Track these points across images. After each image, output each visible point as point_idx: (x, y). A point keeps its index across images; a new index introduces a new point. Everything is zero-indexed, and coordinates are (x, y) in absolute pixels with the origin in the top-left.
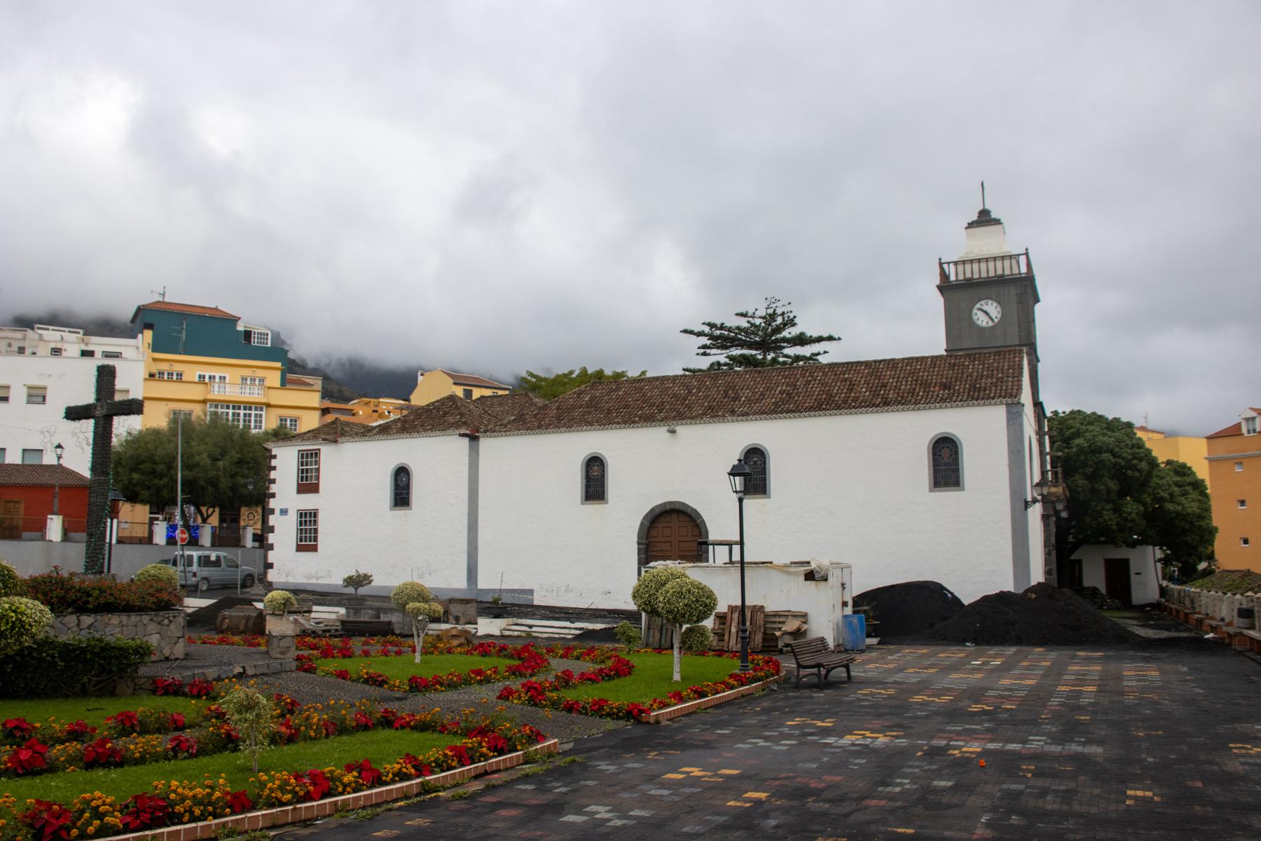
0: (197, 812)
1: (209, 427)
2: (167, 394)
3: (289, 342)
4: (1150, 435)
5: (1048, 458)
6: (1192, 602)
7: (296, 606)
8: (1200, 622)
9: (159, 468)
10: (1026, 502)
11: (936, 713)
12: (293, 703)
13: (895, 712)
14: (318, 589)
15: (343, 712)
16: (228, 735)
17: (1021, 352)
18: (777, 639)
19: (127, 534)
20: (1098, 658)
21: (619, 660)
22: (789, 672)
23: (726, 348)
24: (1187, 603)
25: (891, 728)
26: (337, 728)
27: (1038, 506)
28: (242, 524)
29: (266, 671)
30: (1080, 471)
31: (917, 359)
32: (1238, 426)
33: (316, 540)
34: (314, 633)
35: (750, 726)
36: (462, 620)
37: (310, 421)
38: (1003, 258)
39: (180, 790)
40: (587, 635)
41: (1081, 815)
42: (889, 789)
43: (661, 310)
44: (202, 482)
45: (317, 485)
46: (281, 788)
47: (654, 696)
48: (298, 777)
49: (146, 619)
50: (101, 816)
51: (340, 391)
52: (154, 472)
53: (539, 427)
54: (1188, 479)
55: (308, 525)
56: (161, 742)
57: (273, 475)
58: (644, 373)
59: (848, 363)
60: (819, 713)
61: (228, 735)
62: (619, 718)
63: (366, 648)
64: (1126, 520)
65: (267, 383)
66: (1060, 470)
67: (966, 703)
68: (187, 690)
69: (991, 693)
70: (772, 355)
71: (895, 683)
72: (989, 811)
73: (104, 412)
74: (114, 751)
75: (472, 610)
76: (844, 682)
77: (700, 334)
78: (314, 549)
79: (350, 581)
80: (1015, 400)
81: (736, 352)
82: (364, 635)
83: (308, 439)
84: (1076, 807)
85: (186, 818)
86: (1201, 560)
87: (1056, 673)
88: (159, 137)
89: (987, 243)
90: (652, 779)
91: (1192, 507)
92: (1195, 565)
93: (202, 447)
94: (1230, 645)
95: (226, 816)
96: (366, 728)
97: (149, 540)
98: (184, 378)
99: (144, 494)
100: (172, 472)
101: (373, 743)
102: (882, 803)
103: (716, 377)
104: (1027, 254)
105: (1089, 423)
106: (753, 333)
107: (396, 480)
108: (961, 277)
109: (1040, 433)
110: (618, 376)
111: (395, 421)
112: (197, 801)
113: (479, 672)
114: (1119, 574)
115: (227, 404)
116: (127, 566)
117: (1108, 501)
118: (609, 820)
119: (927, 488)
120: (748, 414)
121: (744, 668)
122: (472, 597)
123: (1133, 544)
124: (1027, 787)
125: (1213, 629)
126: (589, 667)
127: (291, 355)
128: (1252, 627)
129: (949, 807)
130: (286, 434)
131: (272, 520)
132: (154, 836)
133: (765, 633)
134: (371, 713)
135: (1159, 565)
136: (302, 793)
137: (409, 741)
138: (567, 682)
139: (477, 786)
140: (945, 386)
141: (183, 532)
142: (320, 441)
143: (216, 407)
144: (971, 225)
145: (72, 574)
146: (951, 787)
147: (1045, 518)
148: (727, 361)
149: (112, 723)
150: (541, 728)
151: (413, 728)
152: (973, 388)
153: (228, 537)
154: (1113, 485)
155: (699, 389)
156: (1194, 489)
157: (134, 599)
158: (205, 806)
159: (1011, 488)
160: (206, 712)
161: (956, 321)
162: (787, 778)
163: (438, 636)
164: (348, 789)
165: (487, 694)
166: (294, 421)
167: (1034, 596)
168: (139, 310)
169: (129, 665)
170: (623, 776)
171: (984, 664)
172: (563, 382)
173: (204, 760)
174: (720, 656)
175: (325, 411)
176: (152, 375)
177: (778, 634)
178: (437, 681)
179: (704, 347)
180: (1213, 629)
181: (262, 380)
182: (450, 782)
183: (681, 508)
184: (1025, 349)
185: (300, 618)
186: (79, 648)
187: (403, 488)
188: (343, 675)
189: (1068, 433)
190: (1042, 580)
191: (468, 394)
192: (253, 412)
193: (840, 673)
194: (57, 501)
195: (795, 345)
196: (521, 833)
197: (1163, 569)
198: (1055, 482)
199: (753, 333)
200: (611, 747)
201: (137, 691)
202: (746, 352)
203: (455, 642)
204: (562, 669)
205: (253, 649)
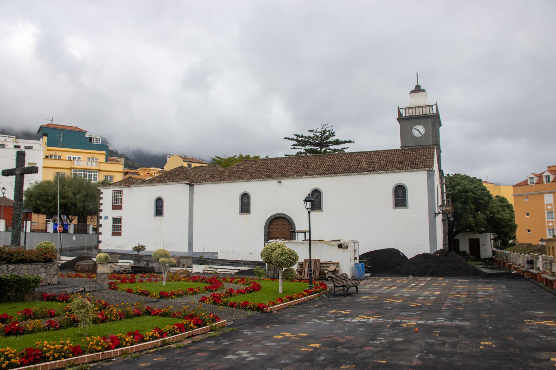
0: (56, 356)
1: (73, 180)
2: (47, 166)
3: (110, 142)
4: (489, 185)
5: (445, 194)
6: (507, 257)
7: (111, 260)
8: (510, 266)
9: (50, 198)
10: (435, 214)
11: (395, 307)
12: (106, 304)
13: (378, 307)
14: (122, 252)
15: (128, 308)
16: (74, 319)
17: (433, 148)
18: (325, 274)
19: (35, 228)
20: (467, 282)
21: (255, 284)
22: (331, 289)
23: (304, 145)
24: (505, 257)
25: (376, 314)
26: (124, 316)
27: (441, 216)
28: (88, 223)
29: (94, 289)
31: (388, 150)
32: (526, 181)
33: (120, 230)
34: (119, 272)
35: (313, 313)
36: (186, 266)
37: (119, 177)
38: (426, 106)
39: (48, 346)
40: (241, 272)
41: (460, 354)
42: (375, 342)
43: (275, 129)
44: (69, 205)
45: (121, 206)
46: (96, 344)
47: (270, 300)
48: (105, 339)
49: (39, 266)
50: (9, 359)
51: (133, 164)
52: (47, 200)
53: (220, 180)
54: (505, 204)
55: (117, 224)
56: (41, 323)
57: (101, 201)
58: (267, 156)
59: (357, 152)
60: (344, 308)
61: (74, 319)
62: (254, 310)
63: (141, 278)
64: (478, 222)
65: (99, 161)
66: (450, 200)
67: (409, 302)
68: (57, 298)
69: (420, 298)
70: (324, 149)
71: (378, 293)
72: (419, 352)
73: (20, 172)
74: (19, 328)
75: (190, 261)
76: (355, 293)
77: (292, 139)
78: (120, 234)
79: (136, 249)
80: (431, 169)
81: (308, 147)
82: (141, 273)
83: (117, 185)
84: (458, 350)
85: (51, 359)
86: (510, 239)
87: (448, 289)
88: (49, 49)
89: (419, 100)
90: (268, 338)
91: (506, 216)
92: (508, 241)
93: (69, 189)
94: (523, 276)
95: (70, 357)
96: (138, 315)
97: (45, 231)
98: (62, 158)
99: (43, 210)
100: (56, 200)
101: (141, 322)
102: (372, 349)
103: (299, 158)
104: (436, 105)
105: (463, 179)
106: (316, 139)
107: (156, 204)
108: (407, 115)
109: (441, 183)
110: (256, 158)
111: (156, 177)
112: (56, 351)
113: (191, 289)
114: (475, 245)
115: (81, 170)
116: (32, 242)
117: (471, 214)
118: (248, 357)
119: (161, 218)
120: (313, 175)
121: (311, 287)
122: (191, 256)
124: (436, 341)
125: (516, 269)
126: (241, 287)
127: (110, 148)
128: (533, 268)
129: (401, 350)
130: (107, 183)
131: (101, 222)
132: (35, 368)
133: (320, 272)
134: (141, 309)
135: (492, 241)
136: (106, 346)
137: (158, 321)
138: (231, 294)
139: (188, 342)
140: (400, 163)
141: (60, 227)
142: (123, 186)
143: (76, 171)
145: (5, 246)
146: (403, 341)
147: (443, 220)
148: (304, 151)
149: (20, 314)
150: (218, 315)
151: (160, 315)
152: (413, 163)
153: (81, 229)
154: (473, 207)
155: (292, 164)
157: (33, 257)
158: (60, 353)
159: (429, 208)
160: (65, 309)
161: (405, 134)
162: (329, 337)
163: (175, 273)
164: (128, 344)
165: (195, 299)
166: (112, 177)
167: (438, 255)
168: (41, 127)
169: (30, 287)
170: (255, 337)
171: (417, 285)
172: (231, 160)
173: (62, 331)
174: (300, 281)
175: (126, 173)
176: (47, 157)
177: (326, 272)
178: (172, 294)
179: (294, 145)
180: (516, 269)
181: (97, 159)
182: (176, 340)
183: (284, 216)
184: (435, 147)
185: (113, 265)
186: (6, 280)
187: (160, 207)
188: (130, 291)
189: (453, 184)
190: (442, 248)
191: (190, 166)
192: (93, 174)
193: (353, 289)
194: (2, 213)
195: (334, 144)
196: (207, 364)
197: (494, 243)
198: (448, 205)
199: (316, 139)
200: (250, 323)
201: (34, 299)
202: (313, 147)
203: (182, 276)
204: (229, 288)
205: (90, 280)
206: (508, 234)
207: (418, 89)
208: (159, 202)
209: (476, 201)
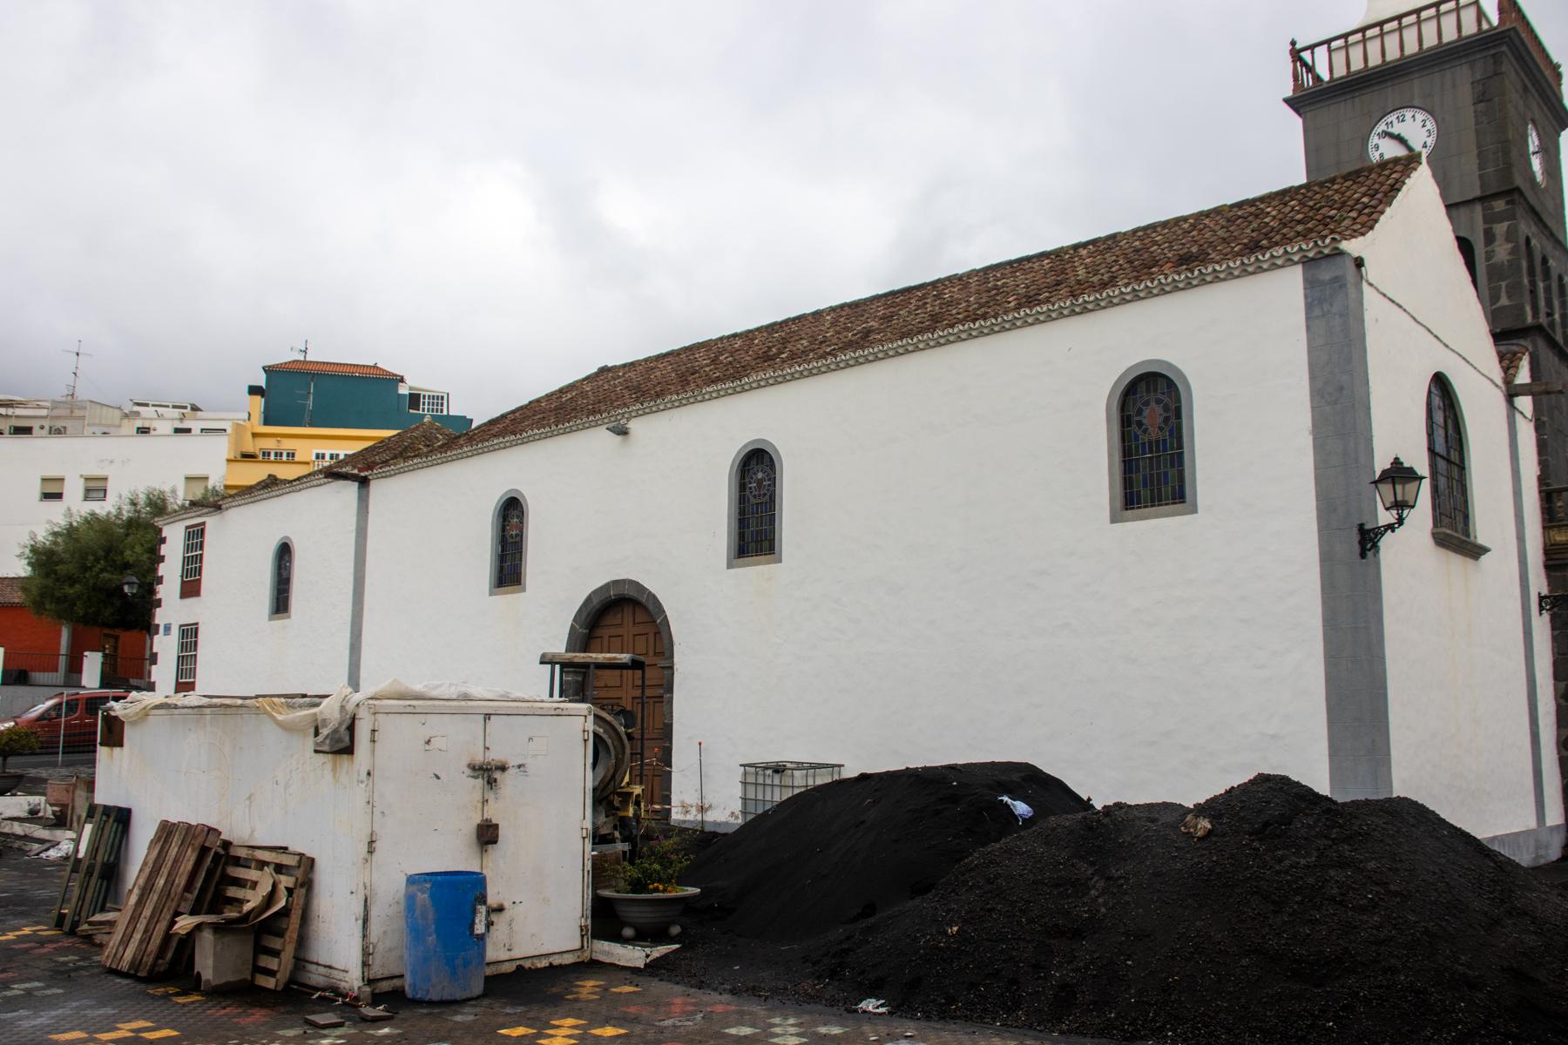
98: (297, 459)
108: (1340, 71)
119: (286, 621)
167: (1205, 824)
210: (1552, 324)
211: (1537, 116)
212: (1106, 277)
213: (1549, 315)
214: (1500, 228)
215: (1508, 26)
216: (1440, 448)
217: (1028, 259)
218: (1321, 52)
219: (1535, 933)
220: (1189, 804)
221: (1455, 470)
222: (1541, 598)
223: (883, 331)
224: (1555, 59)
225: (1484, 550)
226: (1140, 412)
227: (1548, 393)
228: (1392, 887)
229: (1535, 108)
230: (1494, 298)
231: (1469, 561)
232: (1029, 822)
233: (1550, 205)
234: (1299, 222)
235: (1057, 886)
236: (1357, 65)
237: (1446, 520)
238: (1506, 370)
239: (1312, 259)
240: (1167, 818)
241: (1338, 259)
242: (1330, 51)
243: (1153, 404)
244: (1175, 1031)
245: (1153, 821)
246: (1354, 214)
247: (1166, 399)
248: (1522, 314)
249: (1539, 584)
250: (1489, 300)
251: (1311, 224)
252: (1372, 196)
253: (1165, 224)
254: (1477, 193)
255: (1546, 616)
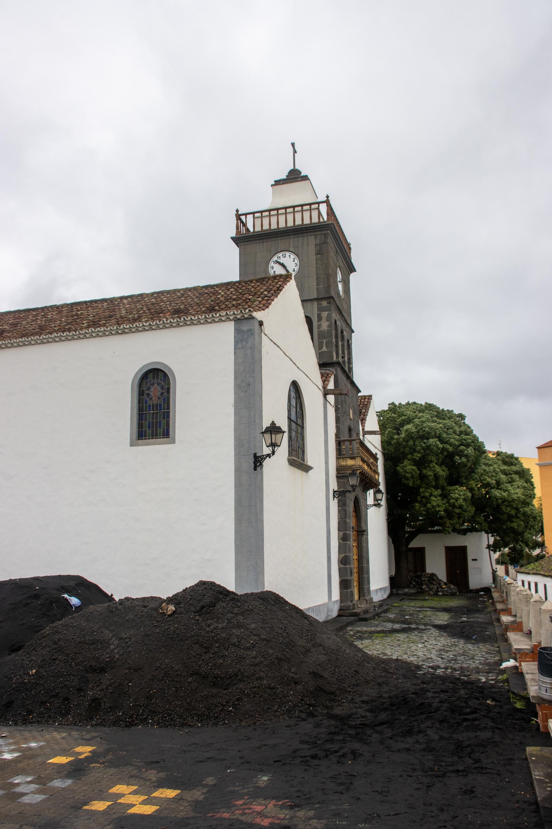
30: (409, 456)
54: (514, 468)
64: (453, 506)
91: (516, 492)
104: (327, 202)
108: (258, 229)
114: (457, 559)
117: (436, 487)
123: (464, 532)
144: (278, 183)
154: (442, 472)
156: (520, 477)
206: (522, 534)
207: (295, 176)
208: (473, 560)
209: (447, 458)
210: (344, 362)
211: (341, 265)
212: (136, 316)
213: (343, 357)
214: (325, 314)
215: (330, 222)
216: (293, 417)
217: (96, 301)
218: (250, 217)
219: (325, 654)
220: (164, 597)
221: (300, 428)
222: (334, 492)
223: (12, 332)
224: (349, 241)
225: (310, 468)
226: (149, 389)
227: (341, 394)
228: (262, 637)
229: (341, 261)
230: (320, 347)
231: (304, 473)
232: (78, 608)
233: (345, 306)
234: (234, 300)
235: (93, 644)
236: (266, 227)
237: (294, 453)
238: (324, 382)
239: (239, 319)
240: (153, 605)
241: (252, 321)
242: (254, 218)
243: (156, 385)
244: (153, 719)
245: (145, 607)
246: (260, 299)
247: (163, 383)
248: (332, 356)
249: (334, 485)
250: (318, 347)
251: (236, 302)
252: (269, 292)
253: (168, 292)
254: (315, 296)
255: (336, 500)
